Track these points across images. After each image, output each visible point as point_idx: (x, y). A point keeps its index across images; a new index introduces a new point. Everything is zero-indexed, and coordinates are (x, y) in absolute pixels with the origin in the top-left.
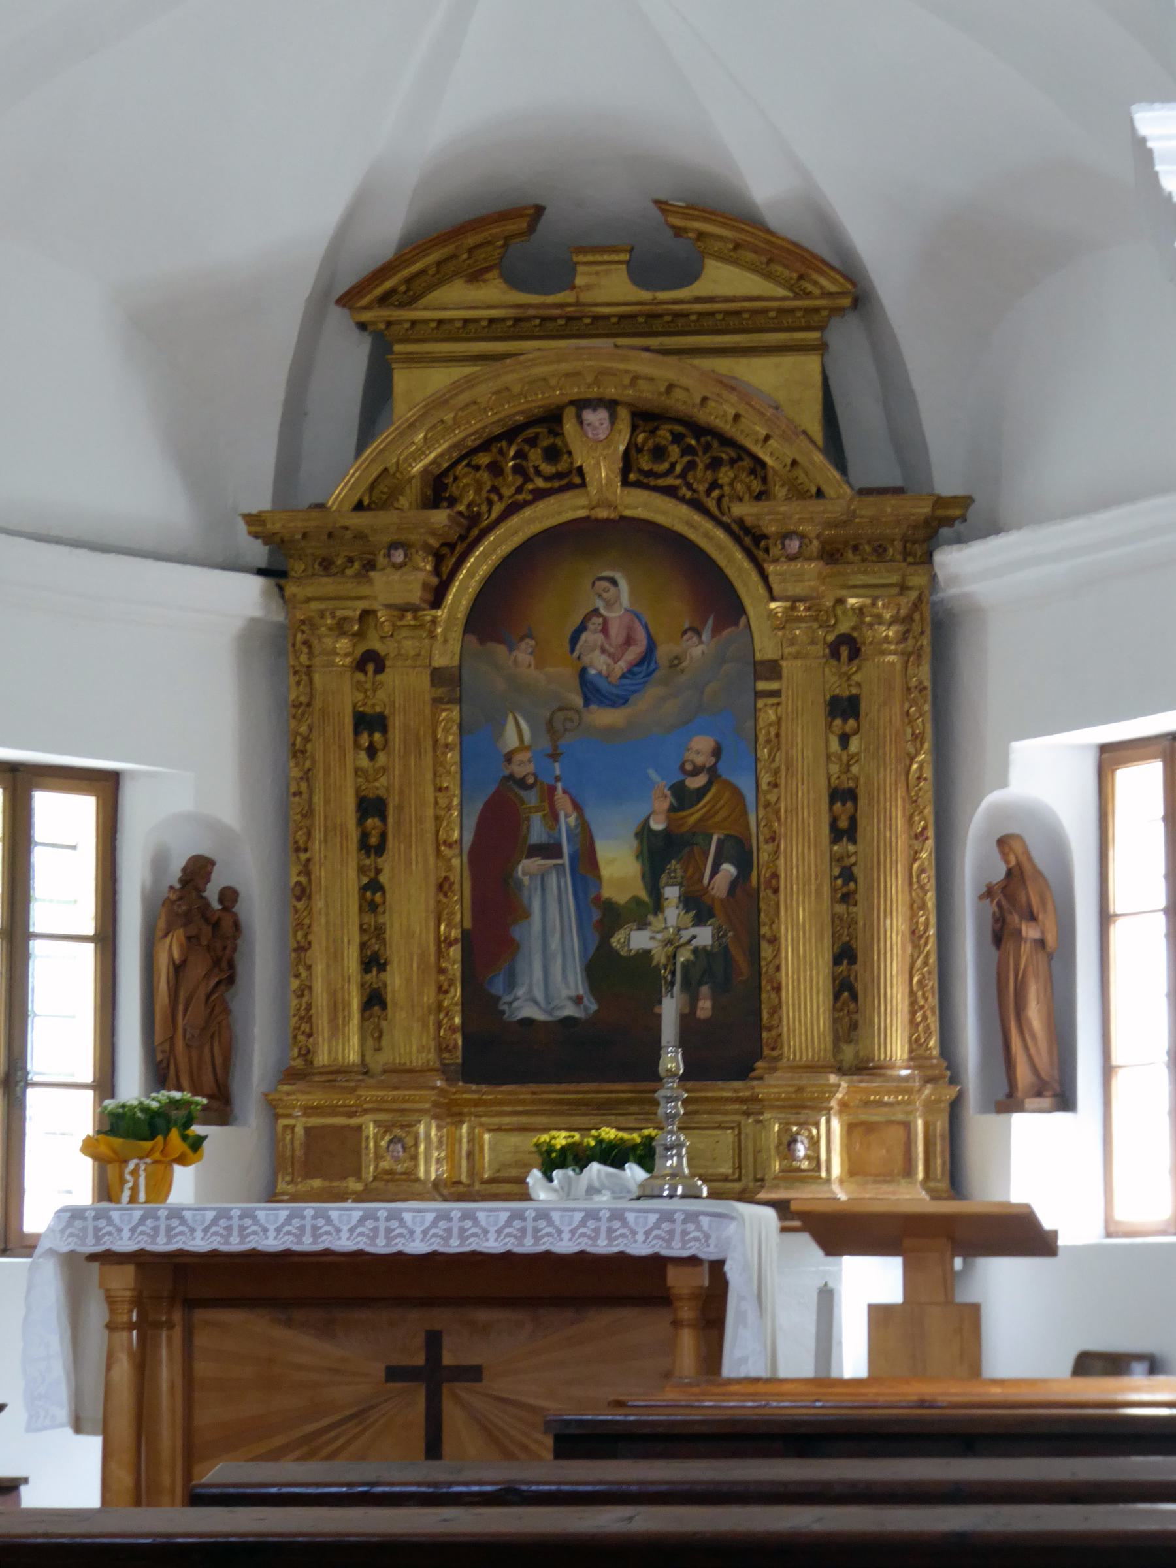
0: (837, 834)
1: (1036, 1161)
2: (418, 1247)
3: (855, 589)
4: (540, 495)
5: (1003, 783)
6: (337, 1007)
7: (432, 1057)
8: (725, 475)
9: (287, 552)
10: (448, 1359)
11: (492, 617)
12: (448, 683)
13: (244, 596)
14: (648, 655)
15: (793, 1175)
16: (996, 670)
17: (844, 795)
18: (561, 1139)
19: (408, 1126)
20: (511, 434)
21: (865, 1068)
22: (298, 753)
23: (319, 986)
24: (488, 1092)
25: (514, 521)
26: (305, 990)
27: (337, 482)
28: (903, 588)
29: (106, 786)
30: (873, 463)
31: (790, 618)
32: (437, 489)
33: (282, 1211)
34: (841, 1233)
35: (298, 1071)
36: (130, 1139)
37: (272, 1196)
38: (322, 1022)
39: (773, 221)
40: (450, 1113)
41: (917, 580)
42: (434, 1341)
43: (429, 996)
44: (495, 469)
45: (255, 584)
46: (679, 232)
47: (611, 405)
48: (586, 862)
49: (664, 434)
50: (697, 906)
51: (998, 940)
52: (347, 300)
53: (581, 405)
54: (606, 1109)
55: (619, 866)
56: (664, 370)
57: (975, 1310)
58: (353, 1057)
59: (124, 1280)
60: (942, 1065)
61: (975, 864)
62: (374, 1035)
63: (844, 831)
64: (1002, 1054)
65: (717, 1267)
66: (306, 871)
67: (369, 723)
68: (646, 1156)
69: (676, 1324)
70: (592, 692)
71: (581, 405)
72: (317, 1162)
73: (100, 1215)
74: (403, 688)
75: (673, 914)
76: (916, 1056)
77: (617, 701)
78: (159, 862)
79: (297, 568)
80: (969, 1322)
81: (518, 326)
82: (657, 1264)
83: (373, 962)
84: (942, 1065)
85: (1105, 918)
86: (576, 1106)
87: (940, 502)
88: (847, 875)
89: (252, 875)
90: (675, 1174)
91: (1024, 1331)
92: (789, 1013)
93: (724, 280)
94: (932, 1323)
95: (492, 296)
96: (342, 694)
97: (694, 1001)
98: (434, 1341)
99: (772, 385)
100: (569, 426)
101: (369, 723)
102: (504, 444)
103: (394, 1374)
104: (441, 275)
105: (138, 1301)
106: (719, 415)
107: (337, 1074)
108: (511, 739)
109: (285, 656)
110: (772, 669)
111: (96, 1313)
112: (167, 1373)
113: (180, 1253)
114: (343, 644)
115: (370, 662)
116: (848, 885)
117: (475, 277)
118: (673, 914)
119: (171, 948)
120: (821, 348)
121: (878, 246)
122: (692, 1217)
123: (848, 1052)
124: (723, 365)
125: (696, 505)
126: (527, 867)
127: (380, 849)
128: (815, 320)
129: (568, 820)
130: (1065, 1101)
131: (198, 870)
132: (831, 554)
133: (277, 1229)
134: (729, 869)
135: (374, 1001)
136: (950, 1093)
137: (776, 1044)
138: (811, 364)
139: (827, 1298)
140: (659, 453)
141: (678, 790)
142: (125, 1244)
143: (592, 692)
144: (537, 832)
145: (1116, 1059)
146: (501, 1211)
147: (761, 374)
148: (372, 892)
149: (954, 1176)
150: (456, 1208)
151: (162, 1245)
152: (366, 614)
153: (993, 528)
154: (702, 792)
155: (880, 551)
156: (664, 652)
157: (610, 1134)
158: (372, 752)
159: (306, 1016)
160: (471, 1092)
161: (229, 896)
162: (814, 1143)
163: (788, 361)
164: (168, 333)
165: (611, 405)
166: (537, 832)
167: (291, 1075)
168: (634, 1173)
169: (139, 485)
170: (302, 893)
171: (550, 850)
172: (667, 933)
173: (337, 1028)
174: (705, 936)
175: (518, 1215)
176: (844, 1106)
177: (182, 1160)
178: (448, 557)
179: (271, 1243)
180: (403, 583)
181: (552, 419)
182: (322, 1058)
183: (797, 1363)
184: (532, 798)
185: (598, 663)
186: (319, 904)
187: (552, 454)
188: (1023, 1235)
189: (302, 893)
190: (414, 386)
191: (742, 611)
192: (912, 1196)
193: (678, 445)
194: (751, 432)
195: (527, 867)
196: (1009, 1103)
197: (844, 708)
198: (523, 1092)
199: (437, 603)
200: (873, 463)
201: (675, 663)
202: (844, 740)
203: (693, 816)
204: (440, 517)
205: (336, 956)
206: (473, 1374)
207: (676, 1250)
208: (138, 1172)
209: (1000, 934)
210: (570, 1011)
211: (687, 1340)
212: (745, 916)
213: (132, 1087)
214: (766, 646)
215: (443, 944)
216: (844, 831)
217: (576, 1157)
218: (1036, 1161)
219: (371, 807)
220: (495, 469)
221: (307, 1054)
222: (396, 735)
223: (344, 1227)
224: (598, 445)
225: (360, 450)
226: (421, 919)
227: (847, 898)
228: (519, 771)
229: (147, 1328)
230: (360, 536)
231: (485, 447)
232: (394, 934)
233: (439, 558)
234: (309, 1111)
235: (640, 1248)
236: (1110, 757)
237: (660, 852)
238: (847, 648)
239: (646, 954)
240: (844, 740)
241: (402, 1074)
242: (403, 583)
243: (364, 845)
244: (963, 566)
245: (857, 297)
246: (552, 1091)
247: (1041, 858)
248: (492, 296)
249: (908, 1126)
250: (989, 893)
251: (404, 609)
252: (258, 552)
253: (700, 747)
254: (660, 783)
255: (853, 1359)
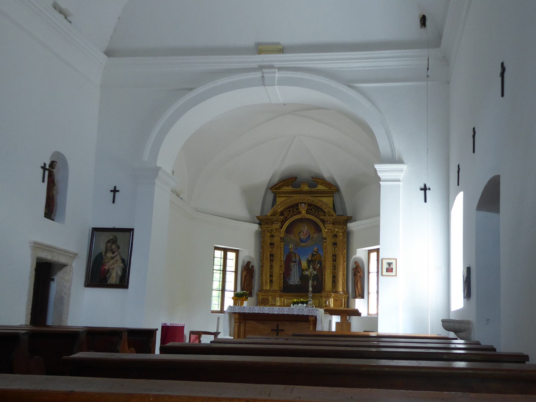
0: (333, 261)
1: (359, 304)
2: (276, 313)
3: (337, 228)
4: (295, 215)
5: (356, 254)
6: (266, 282)
7: (279, 289)
8: (320, 213)
9: (262, 221)
10: (279, 328)
11: (289, 231)
12: (282, 239)
13: (256, 227)
14: (309, 235)
15: (326, 306)
16: (355, 239)
17: (334, 256)
18: (295, 300)
19: (275, 298)
20: (292, 207)
21: (336, 292)
22: (262, 248)
23: (264, 279)
24: (286, 294)
25: (292, 218)
26: (262, 279)
27: (269, 212)
28: (343, 228)
29: (237, 252)
30: (339, 212)
31: (328, 232)
32: (282, 214)
33: (258, 307)
34: (332, 312)
35: (261, 290)
36: (238, 297)
37: (257, 306)
38: (264, 284)
39: (327, 180)
40: (281, 296)
41: (345, 227)
42: (278, 326)
43: (279, 281)
44: (289, 211)
45: (257, 225)
46: (314, 181)
47: (305, 203)
48: (300, 264)
49: (312, 207)
50: (315, 269)
51: (354, 276)
52: (271, 189)
53: (301, 203)
54: (302, 297)
55: (304, 264)
56: (312, 199)
57: (350, 323)
58: (268, 288)
59: (237, 316)
60: (346, 292)
61: (351, 265)
62: (271, 285)
63: (334, 260)
64: (354, 291)
65: (316, 317)
66: (263, 263)
67: (272, 244)
68: (307, 303)
69: (310, 324)
70: (301, 241)
71: (301, 203)
72: (263, 302)
73: (234, 307)
74: (276, 240)
75: (311, 269)
76: (343, 291)
77: (305, 242)
78: (243, 262)
79: (263, 223)
80: (349, 325)
81: (293, 193)
82: (308, 316)
83: (271, 276)
84: (346, 292)
85: (369, 273)
86: (297, 296)
87: (348, 217)
88: (335, 266)
89: (256, 264)
90: (311, 304)
91: (356, 326)
92: (326, 285)
93: (320, 187)
94: (344, 325)
95: (290, 189)
96: (268, 240)
97: (314, 282)
98: (278, 326)
99: (327, 200)
100: (299, 206)
101: (272, 244)
102: (277, 70)
103: (272, 330)
104: (283, 185)
105: (239, 319)
106: (319, 205)
107: (266, 291)
108: (290, 247)
109: (261, 235)
110: (325, 239)
111: (233, 320)
112: (242, 329)
113: (244, 313)
114: (269, 234)
115: (272, 236)
116: (335, 268)
117: (288, 186)
118: (311, 269)
119: (245, 273)
120: (333, 196)
121: (340, 183)
122: (312, 310)
123: (334, 290)
124: (320, 198)
125: (316, 217)
126: (292, 264)
127: (273, 261)
128: (332, 193)
129: (298, 258)
130: (363, 297)
131: (249, 263)
132: (334, 223)
133: (258, 310)
134: (319, 265)
135: (271, 281)
136: (347, 296)
137: (325, 289)
138: (332, 199)
139: (330, 322)
140: (311, 210)
141: (312, 254)
142: (237, 311)
143: (301, 241)
144: (293, 259)
145: (370, 291)
146: (287, 308)
147: (325, 200)
148: (271, 266)
149: (348, 304)
150: (281, 308)
151: (242, 312)
152: (272, 230)
153: (355, 221)
154: (315, 255)
155: (340, 224)
156: (311, 236)
157: (302, 300)
158: (272, 248)
159: (262, 283)
160: (284, 294)
161: (253, 267)
162: (329, 302)
163: (328, 198)
164: (247, 192)
165: (305, 203)
166: (293, 259)
167: (260, 291)
168: (305, 305)
169: (244, 213)
170: (262, 267)
171: (295, 262)
172: (310, 272)
173: (266, 285)
174: (315, 272)
175: (289, 309)
176: (333, 297)
177: (245, 300)
178: (283, 222)
179: (256, 312)
180: (277, 226)
181: (297, 205)
182: (264, 288)
183: (326, 329)
184: (293, 255)
185: (302, 237)
186: (264, 268)
187: (297, 209)
188: (357, 313)
189: (262, 267)
190: (279, 200)
191: (321, 231)
192: (343, 308)
193: (314, 208)
194: (323, 207)
195: (292, 264)
196: (355, 297)
197: (335, 244)
198: (291, 294)
199: (281, 228)
200: (339, 212)
201: (312, 237)
202: (335, 248)
203: (314, 258)
204: (282, 217)
205: (266, 275)
206: (283, 330)
207: (310, 314)
208: (239, 302)
209: (355, 275)
210: (297, 283)
211: (311, 327)
212: (321, 270)
213: (239, 290)
214: (324, 236)
215: (280, 274)
216: (334, 260)
217: (297, 303)
218: (359, 304)
219: (272, 255)
220: (289, 211)
221: (262, 288)
222: (275, 246)
223: (266, 310)
224: (303, 209)
225: (272, 207)
226: (278, 270)
227: (335, 269)
228: (291, 251)
229: (240, 323)
230: (271, 219)
231: (288, 208)
232: (274, 273)
233: (282, 223)
234: (262, 296)
235: (305, 314)
236: (370, 251)
237: (309, 262)
238: (335, 236)
239: (307, 275)
240: (335, 248)
241: (274, 291)
242: (278, 226)
243: (271, 261)
244: (351, 226)
245: (338, 190)
246: (294, 294)
247: (360, 263)
248: (290, 189)
249: (342, 300)
250: (353, 269)
251: (277, 229)
252: (258, 221)
253: (315, 249)
254: (310, 254)
255: (334, 329)
